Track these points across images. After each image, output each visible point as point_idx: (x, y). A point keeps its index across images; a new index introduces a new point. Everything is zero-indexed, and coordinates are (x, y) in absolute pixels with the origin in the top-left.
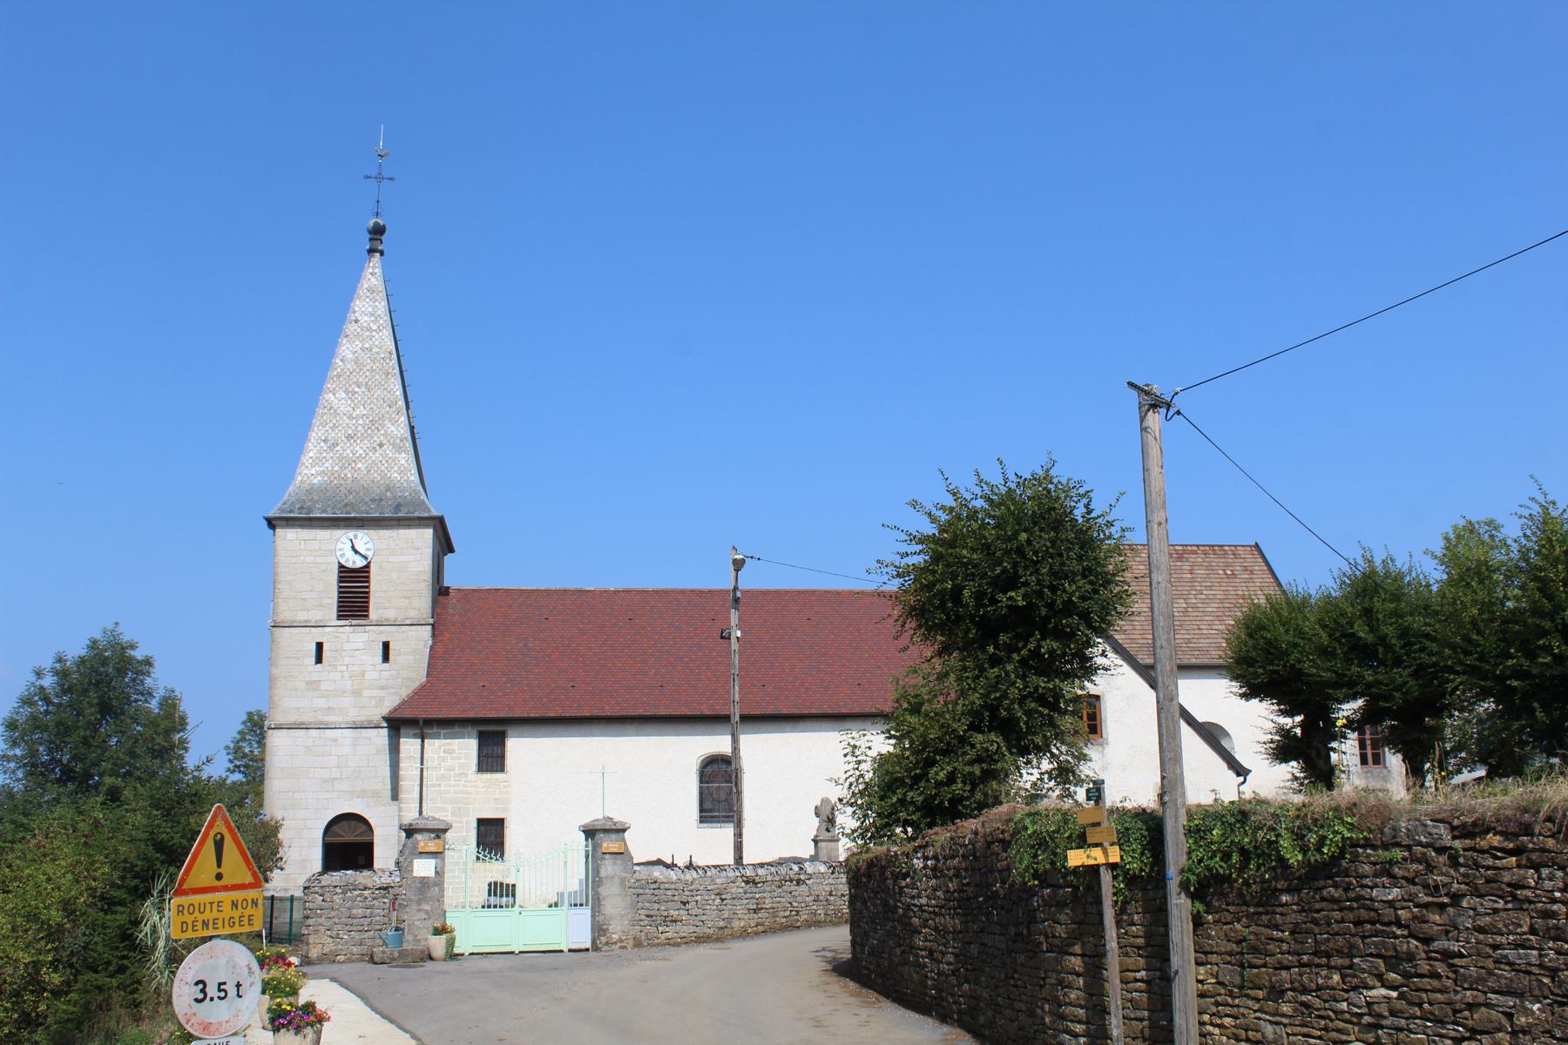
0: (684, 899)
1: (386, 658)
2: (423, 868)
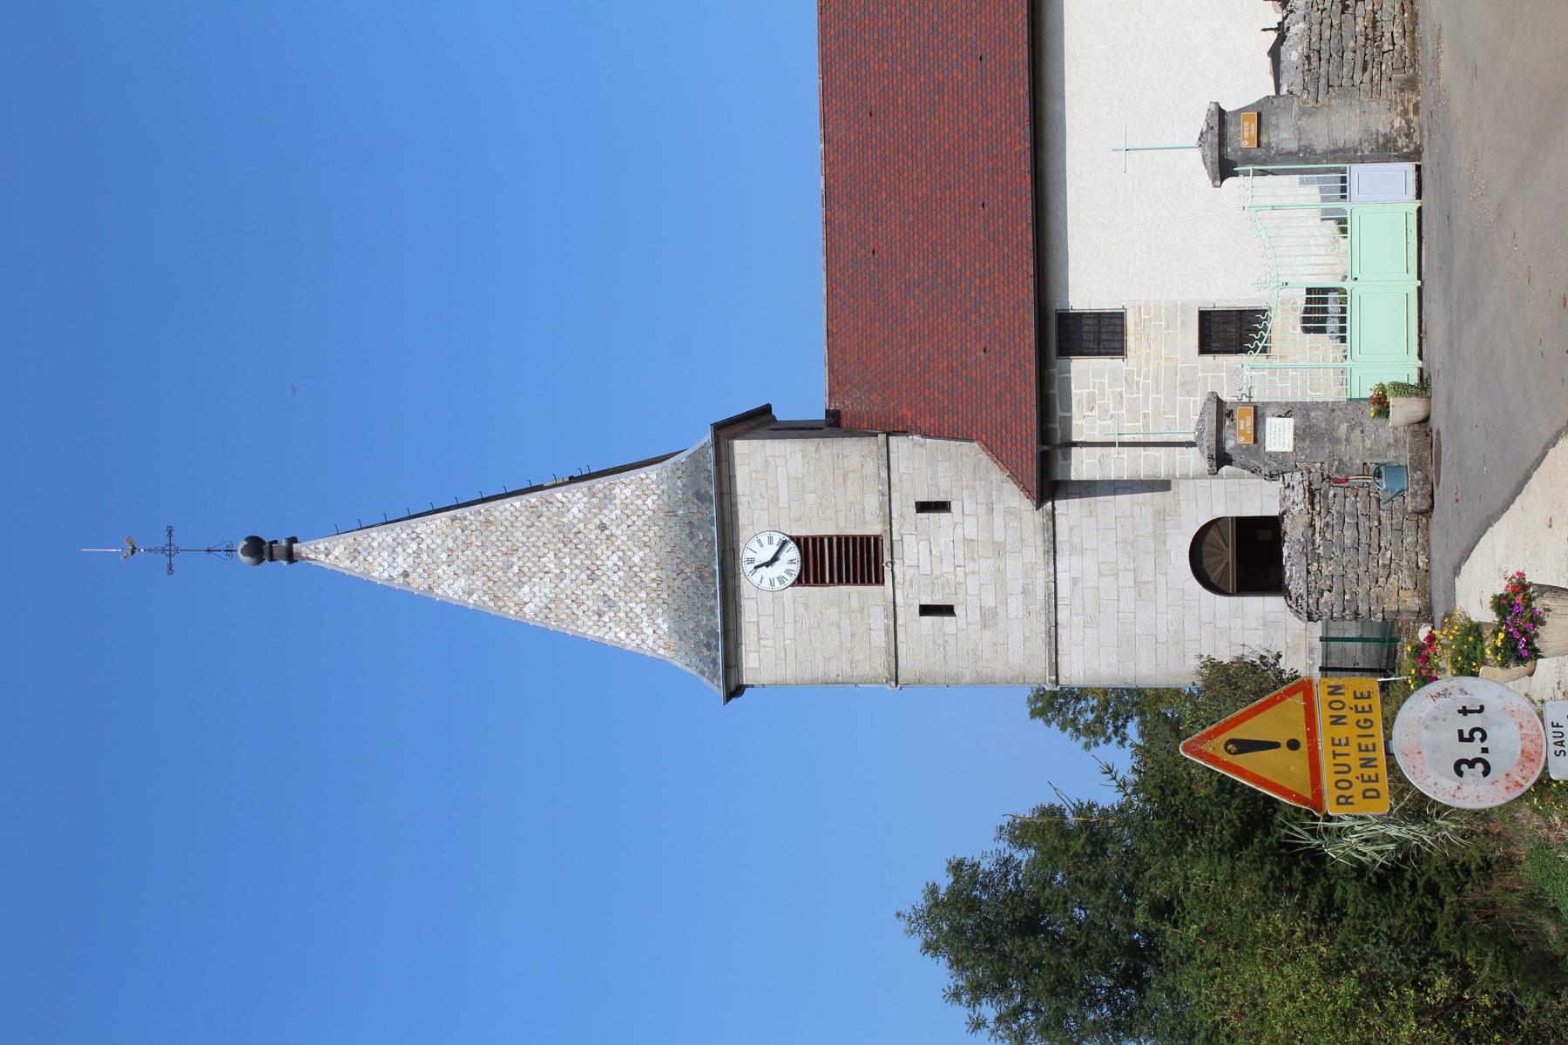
1: (942, 507)
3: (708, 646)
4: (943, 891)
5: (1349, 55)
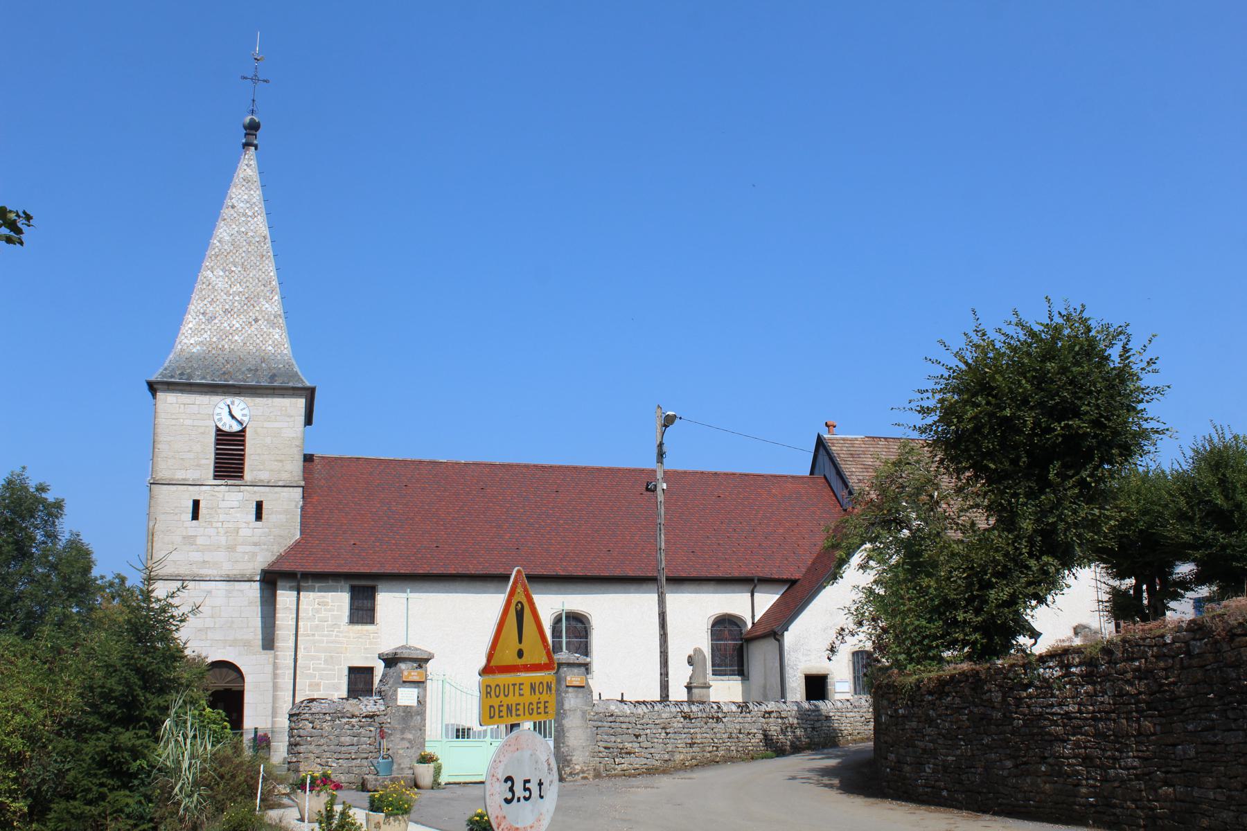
1: (259, 516)
3: (182, 374)
4: (44, 495)
5: (613, 738)
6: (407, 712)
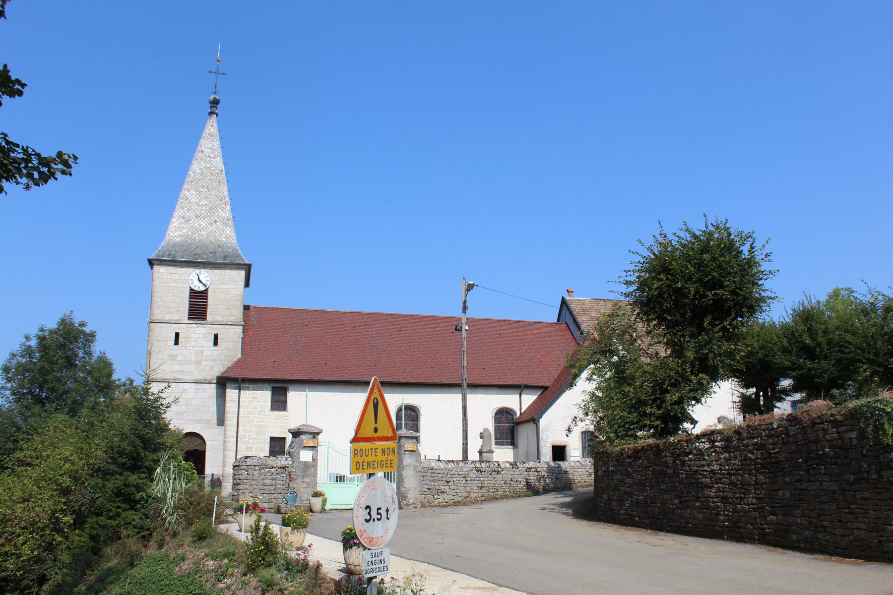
0: (448, 479)
1: (216, 343)
2: (305, 456)
5: (433, 483)
6: (306, 464)
